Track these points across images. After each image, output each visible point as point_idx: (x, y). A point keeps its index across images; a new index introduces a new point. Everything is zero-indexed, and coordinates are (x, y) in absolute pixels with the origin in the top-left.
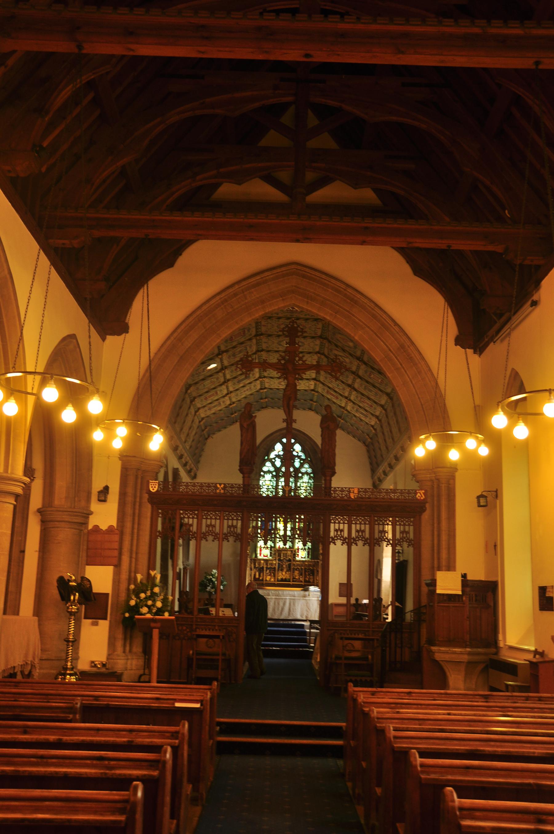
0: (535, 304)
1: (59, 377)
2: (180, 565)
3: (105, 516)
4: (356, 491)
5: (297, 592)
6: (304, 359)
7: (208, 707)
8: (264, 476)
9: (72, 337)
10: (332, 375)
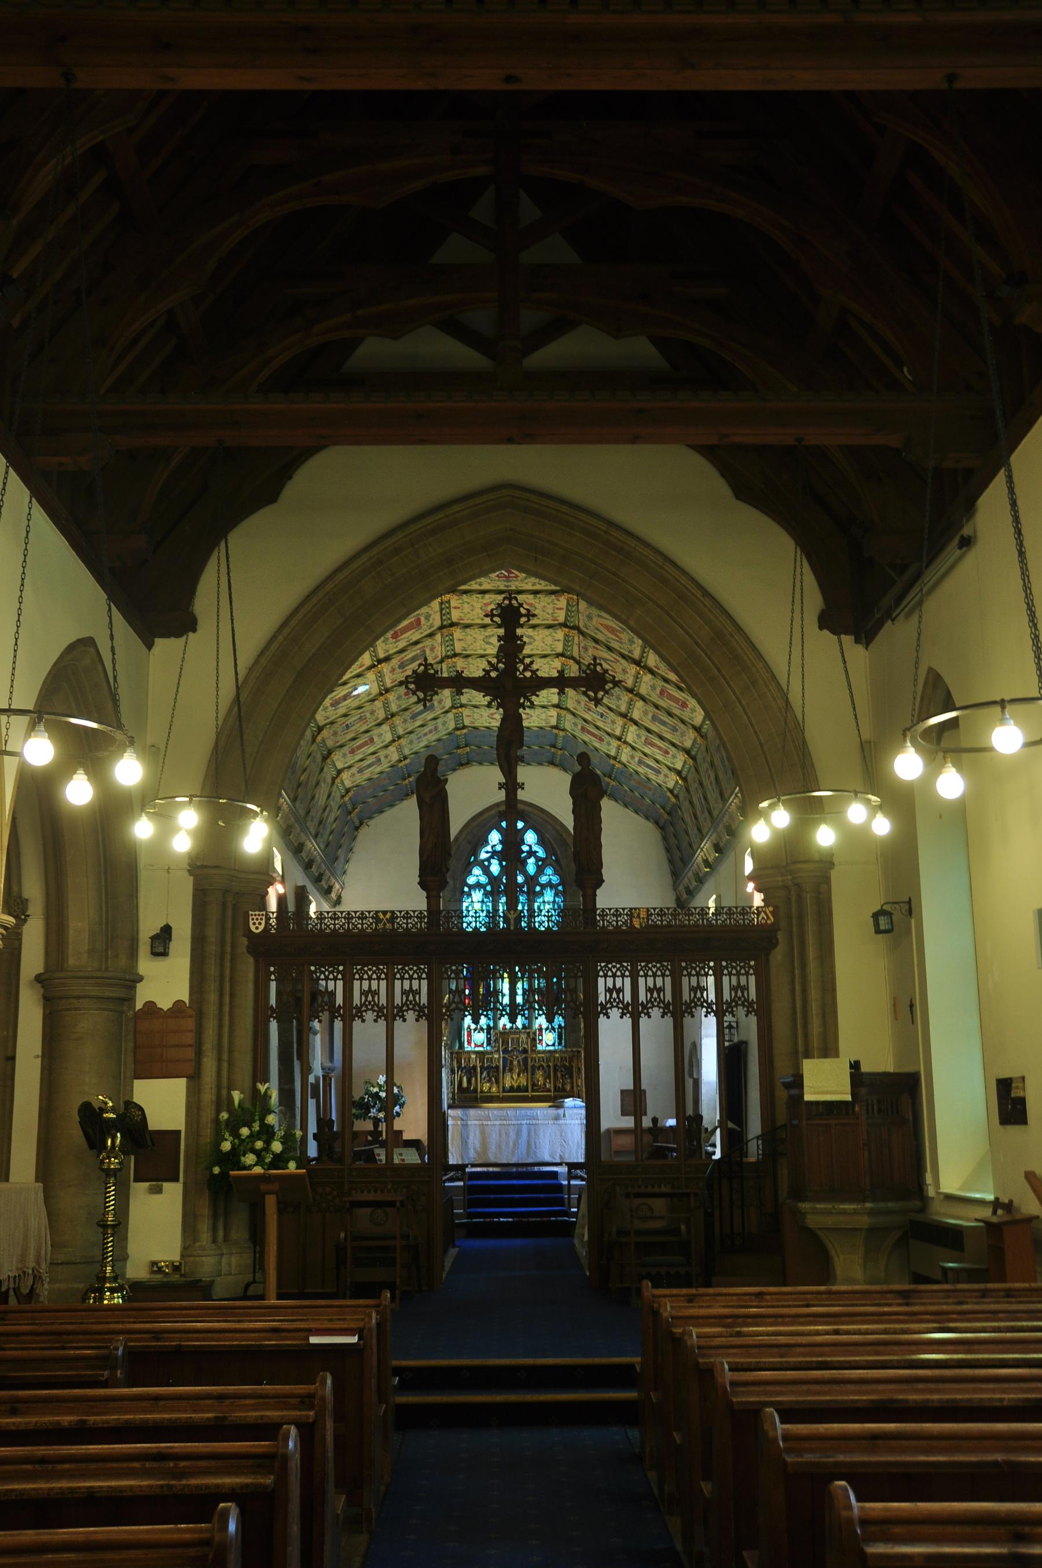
0: (967, 543)
1: (53, 717)
2: (317, 1071)
3: (165, 983)
4: (643, 915)
5: (541, 1110)
6: (535, 667)
7: (374, 1341)
8: (469, 895)
9: (88, 642)
10: (588, 696)
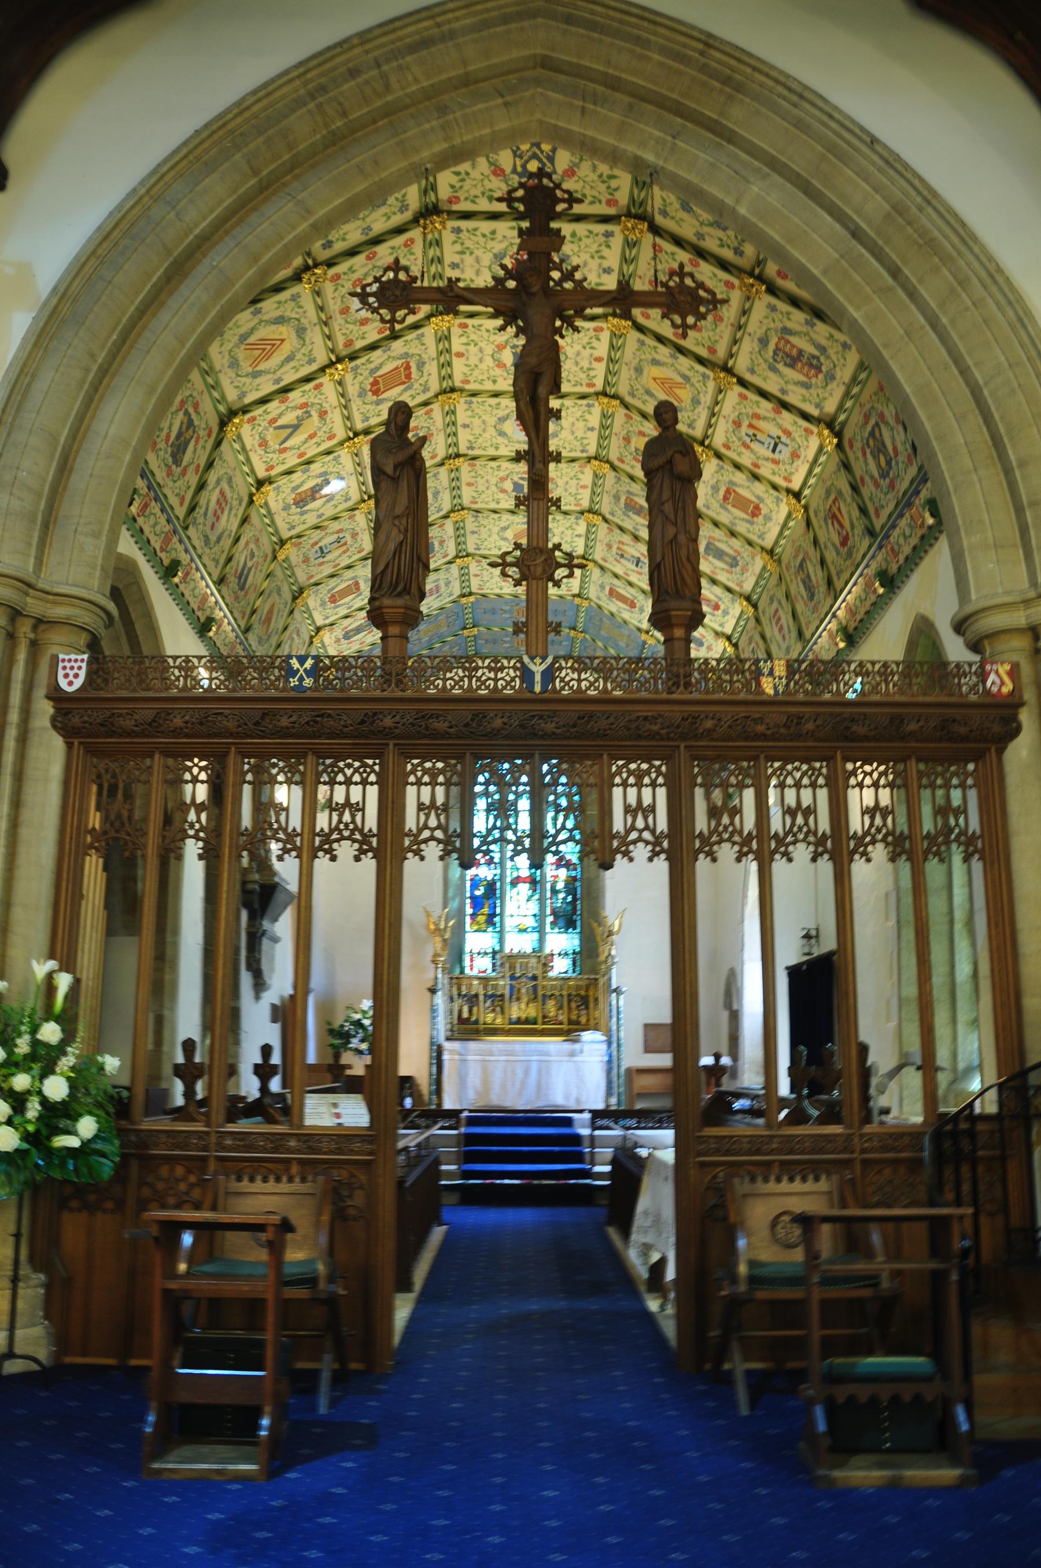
5: (554, 1045)
